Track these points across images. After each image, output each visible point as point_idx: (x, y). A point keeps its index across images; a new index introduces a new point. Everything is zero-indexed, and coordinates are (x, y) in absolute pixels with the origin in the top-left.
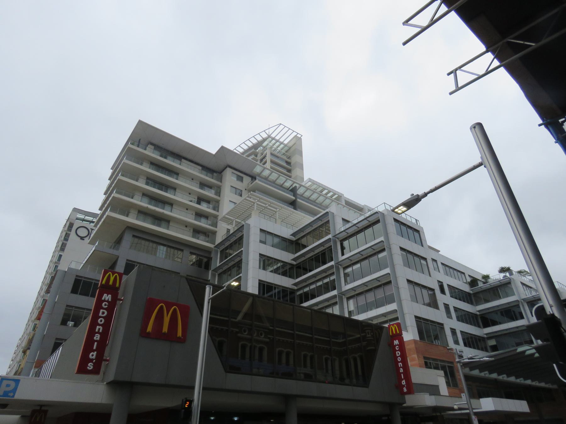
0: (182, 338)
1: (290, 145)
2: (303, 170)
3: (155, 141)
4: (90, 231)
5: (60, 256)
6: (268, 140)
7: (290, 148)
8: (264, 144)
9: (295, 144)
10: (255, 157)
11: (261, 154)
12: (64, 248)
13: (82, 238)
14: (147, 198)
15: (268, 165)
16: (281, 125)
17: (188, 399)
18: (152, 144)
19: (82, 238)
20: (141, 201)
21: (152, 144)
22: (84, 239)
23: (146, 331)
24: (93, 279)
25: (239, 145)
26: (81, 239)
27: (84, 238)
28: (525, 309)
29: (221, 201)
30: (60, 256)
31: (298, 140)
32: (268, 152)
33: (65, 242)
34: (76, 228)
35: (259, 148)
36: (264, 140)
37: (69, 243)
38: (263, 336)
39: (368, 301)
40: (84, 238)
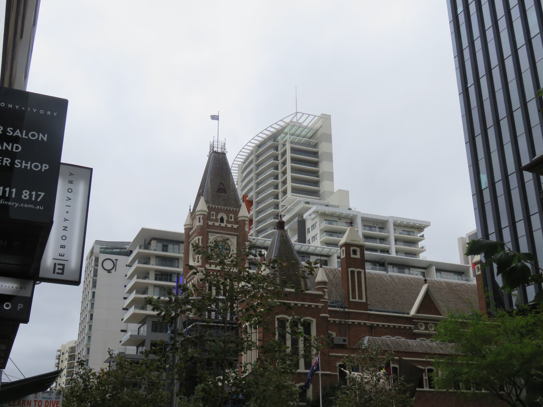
0: (227, 295)
1: (317, 126)
4: (115, 261)
5: (94, 293)
6: (288, 127)
7: (317, 131)
9: (321, 127)
12: (158, 279)
13: (109, 271)
15: (289, 165)
19: (109, 271)
20: (173, 252)
23: (9, 150)
25: (245, 144)
26: (109, 272)
27: (111, 271)
28: (175, 278)
29: (328, 138)
30: (94, 293)
31: (326, 119)
32: (288, 147)
33: (95, 278)
34: (101, 263)
37: (99, 279)
39: (366, 263)
40: (111, 271)
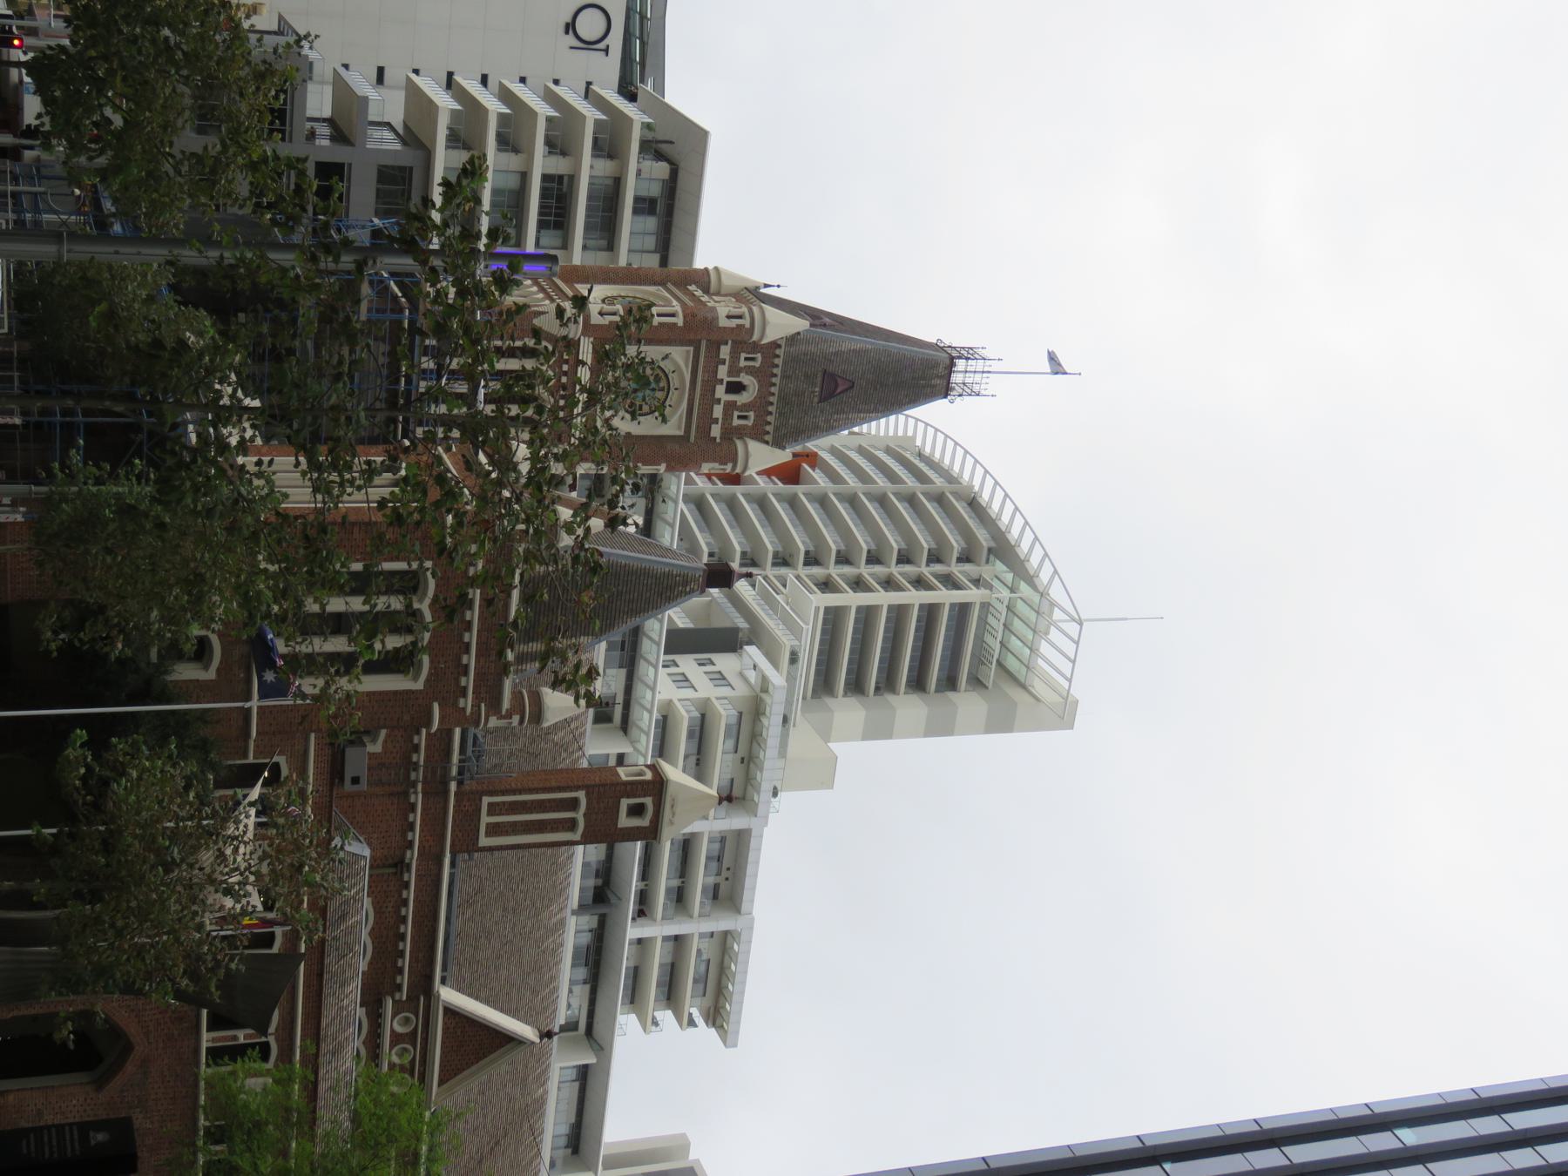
2: (926, 735)
3: (681, 175)
4: (602, 45)
8: (1023, 586)
9: (1038, 700)
10: (955, 555)
11: (975, 576)
13: (570, 27)
14: (519, 183)
16: (1078, 627)
17: (188, 151)
18: (674, 173)
19: (570, 27)
21: (674, 173)
22: (567, 32)
24: (291, 126)
26: (567, 25)
27: (571, 32)
31: (1063, 715)
35: (1005, 568)
36: (1031, 580)
38: (399, 1029)
40: (571, 32)
